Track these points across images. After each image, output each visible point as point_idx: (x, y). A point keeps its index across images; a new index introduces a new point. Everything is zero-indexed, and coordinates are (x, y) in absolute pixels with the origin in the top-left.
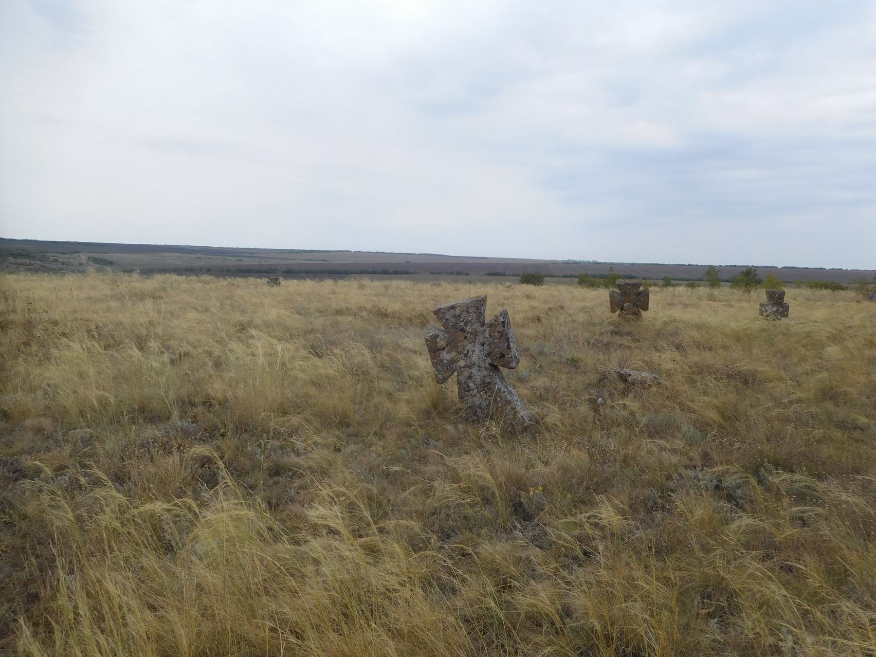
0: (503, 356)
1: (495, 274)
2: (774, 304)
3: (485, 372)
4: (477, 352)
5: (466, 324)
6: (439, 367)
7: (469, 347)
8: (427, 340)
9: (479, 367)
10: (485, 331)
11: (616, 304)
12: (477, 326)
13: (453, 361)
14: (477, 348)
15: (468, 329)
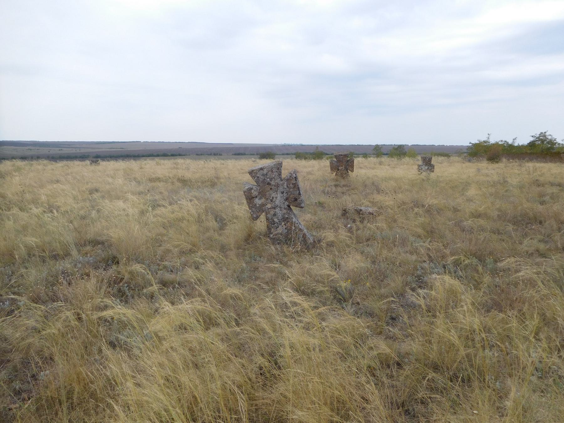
0: (296, 200)
1: (239, 154)
2: (426, 165)
3: (285, 211)
4: (279, 198)
5: (271, 180)
6: (254, 209)
7: (274, 195)
8: (244, 192)
9: (280, 208)
10: (284, 183)
11: (334, 168)
12: (278, 181)
13: (263, 205)
14: (279, 195)
15: (273, 183)
